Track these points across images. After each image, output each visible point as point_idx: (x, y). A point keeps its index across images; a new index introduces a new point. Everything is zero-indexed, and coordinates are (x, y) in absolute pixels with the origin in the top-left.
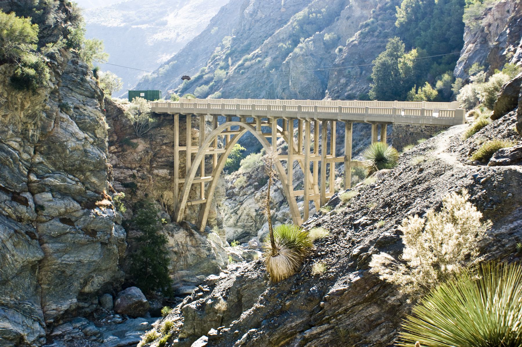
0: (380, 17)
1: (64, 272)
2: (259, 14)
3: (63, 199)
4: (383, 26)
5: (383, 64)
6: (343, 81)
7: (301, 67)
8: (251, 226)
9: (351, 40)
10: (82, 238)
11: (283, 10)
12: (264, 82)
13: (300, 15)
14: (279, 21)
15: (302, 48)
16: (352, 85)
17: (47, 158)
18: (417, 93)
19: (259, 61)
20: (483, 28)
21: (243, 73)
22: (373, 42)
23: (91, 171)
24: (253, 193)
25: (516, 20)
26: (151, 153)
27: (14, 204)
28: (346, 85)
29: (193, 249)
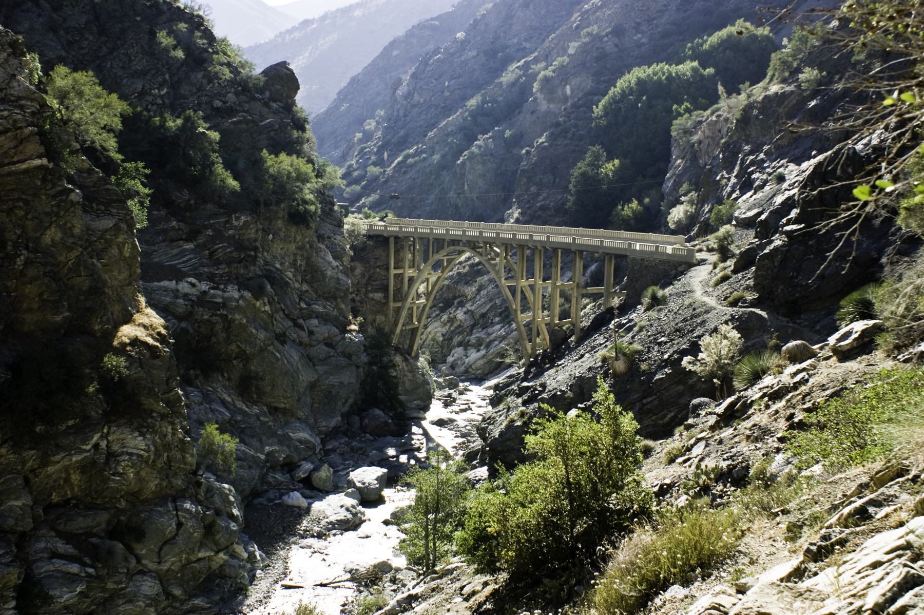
0: (573, 116)
1: (330, 392)
2: (416, 97)
3: (325, 324)
4: (576, 126)
5: (583, 174)
6: (533, 189)
7: (479, 168)
8: (437, 352)
9: (540, 141)
10: (343, 361)
11: (447, 94)
12: (432, 184)
13: (473, 102)
14: (443, 108)
15: (479, 147)
16: (544, 195)
17: (312, 287)
18: (623, 210)
19: (424, 158)
20: (694, 144)
21: (405, 172)
22: (566, 145)
23: (341, 297)
24: (437, 315)
25: (729, 145)
26: (367, 277)
27: (297, 329)
28: (538, 194)
29: (409, 374)
